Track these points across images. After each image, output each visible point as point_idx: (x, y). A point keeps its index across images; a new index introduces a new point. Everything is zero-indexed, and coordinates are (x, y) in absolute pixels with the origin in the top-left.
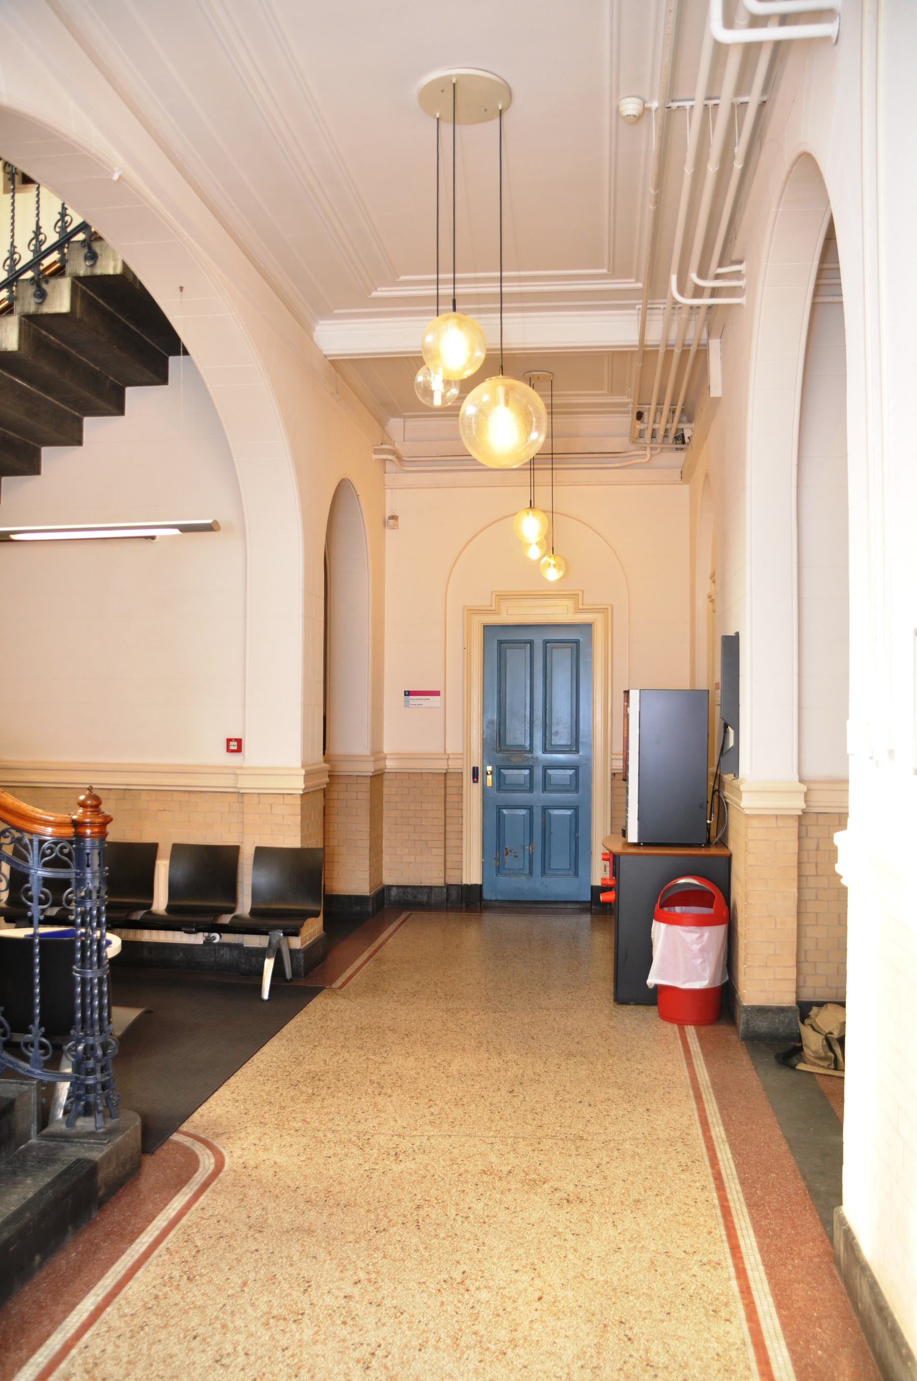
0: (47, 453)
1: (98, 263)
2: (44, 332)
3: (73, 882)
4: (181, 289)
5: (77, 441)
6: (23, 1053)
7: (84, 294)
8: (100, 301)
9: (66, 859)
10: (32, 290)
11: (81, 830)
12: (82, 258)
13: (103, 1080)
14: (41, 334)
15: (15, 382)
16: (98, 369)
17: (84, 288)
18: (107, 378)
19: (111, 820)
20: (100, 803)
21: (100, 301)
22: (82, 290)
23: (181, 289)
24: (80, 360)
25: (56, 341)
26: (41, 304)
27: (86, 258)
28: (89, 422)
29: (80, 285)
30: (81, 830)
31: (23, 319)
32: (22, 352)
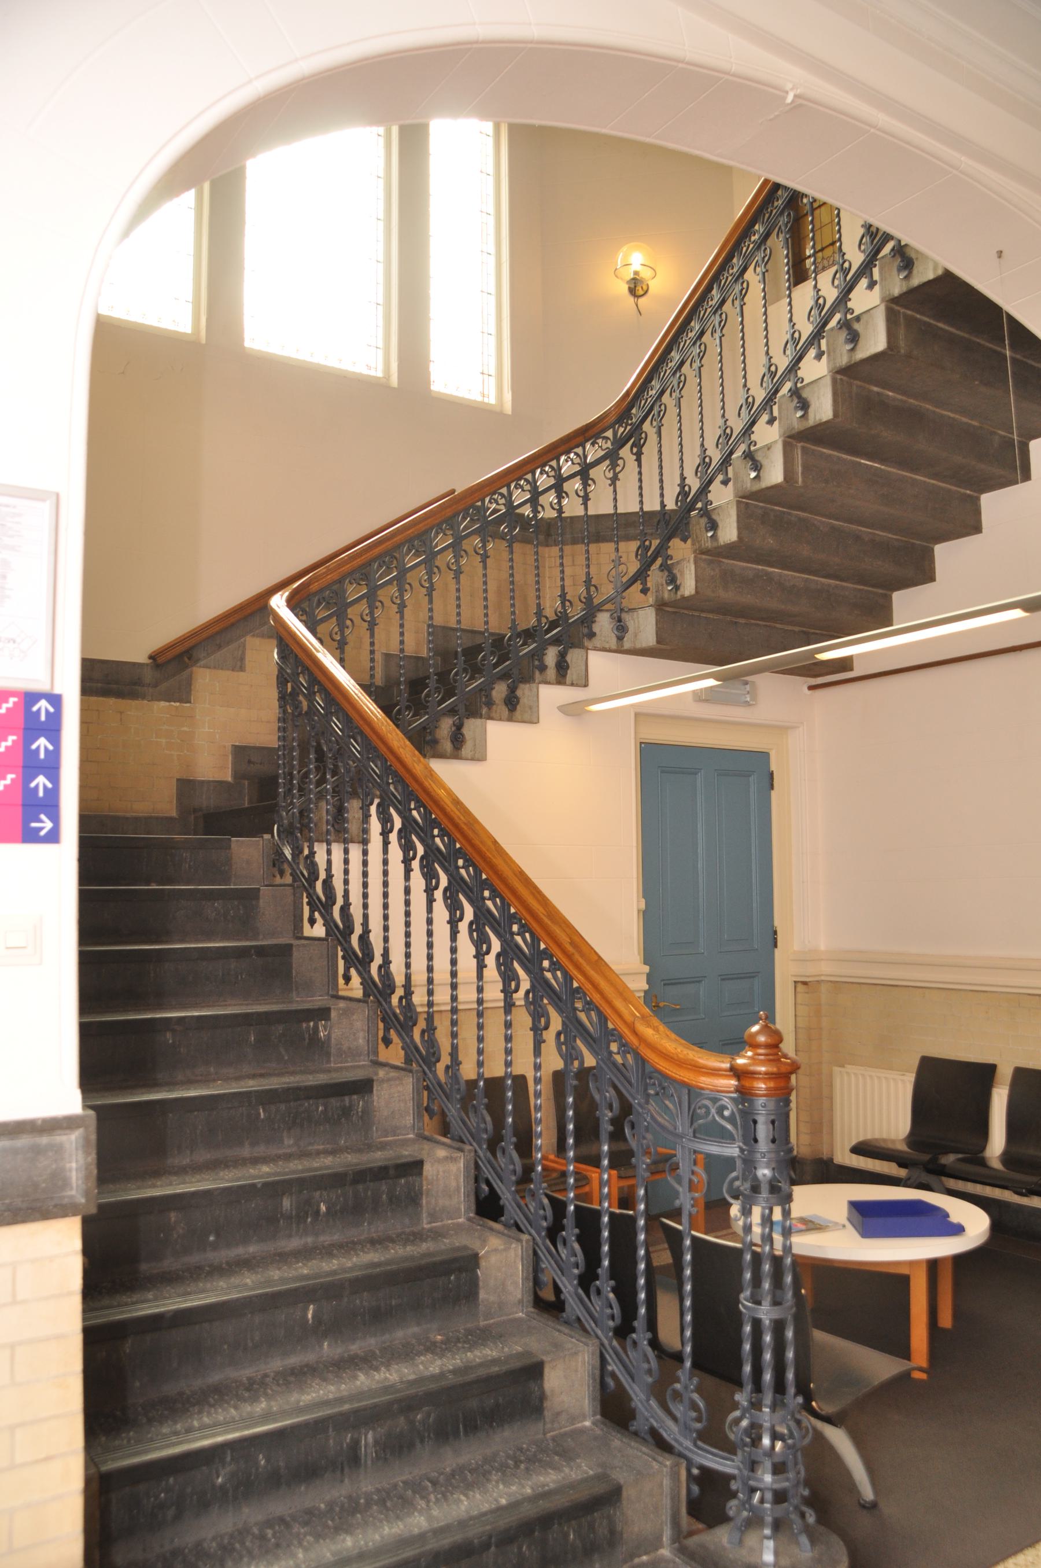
0: (942, 552)
1: (915, 271)
2: (876, 389)
3: (739, 1163)
4: (1000, 254)
5: (976, 528)
6: (666, 1402)
7: (910, 321)
8: (941, 325)
9: (729, 1127)
10: (843, 335)
11: (747, 1083)
12: (895, 272)
13: (776, 1486)
14: (870, 391)
15: (860, 463)
16: (975, 423)
17: (909, 312)
18: (993, 433)
19: (799, 1068)
20: (781, 1041)
21: (941, 325)
22: (905, 316)
23: (1000, 254)
24: (942, 416)
25: (899, 397)
26: (853, 350)
27: (900, 270)
28: (989, 501)
29: (902, 310)
30: (747, 1083)
31: (839, 377)
32: (840, 419)
